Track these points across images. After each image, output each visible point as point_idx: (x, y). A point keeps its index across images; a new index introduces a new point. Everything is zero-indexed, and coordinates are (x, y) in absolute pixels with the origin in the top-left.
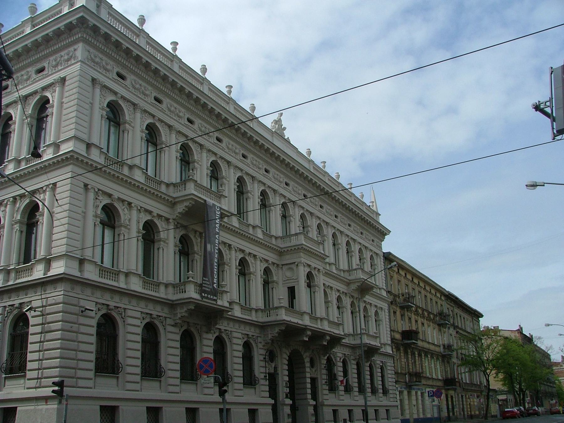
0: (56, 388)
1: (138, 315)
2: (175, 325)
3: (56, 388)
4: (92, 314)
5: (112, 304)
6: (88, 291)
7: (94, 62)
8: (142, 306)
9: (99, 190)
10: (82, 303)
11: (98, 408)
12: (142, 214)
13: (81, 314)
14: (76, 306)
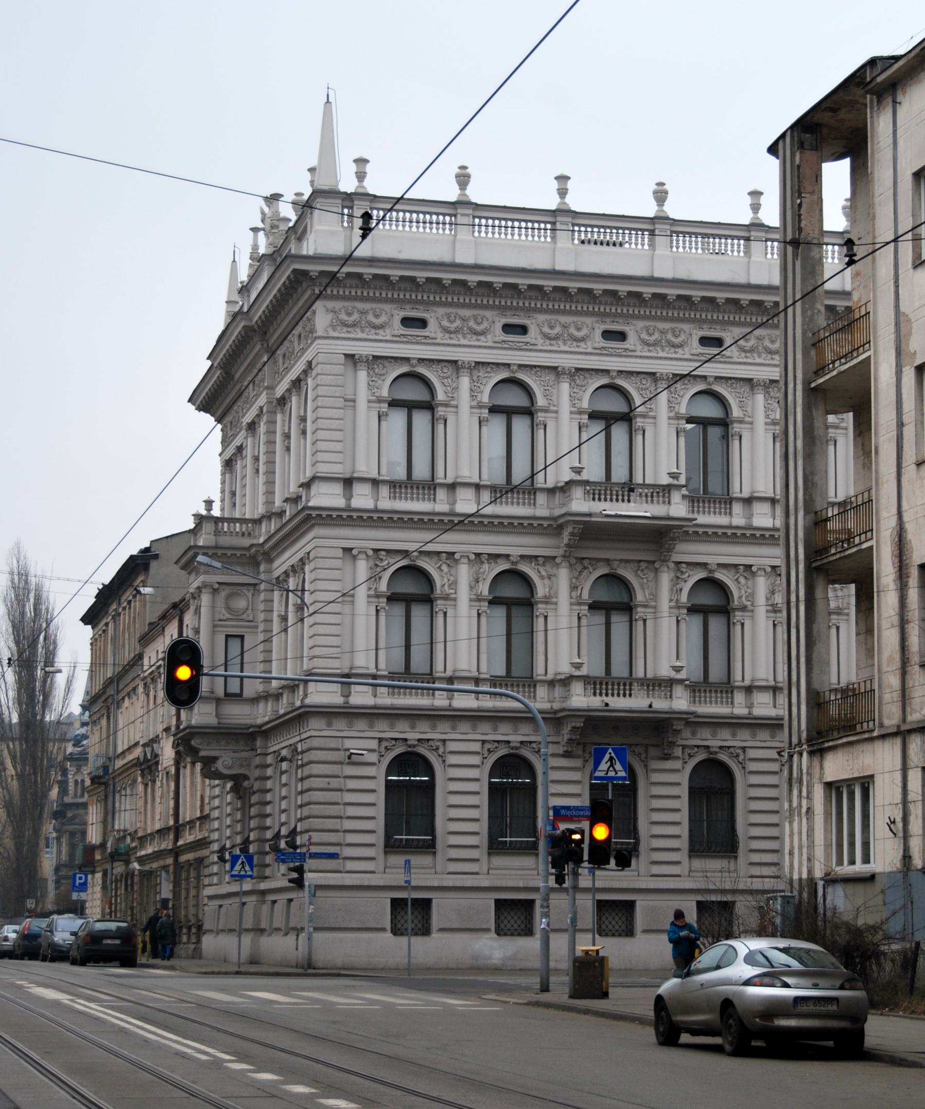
0: (295, 875)
1: (476, 747)
2: (567, 755)
3: (295, 875)
4: (373, 757)
5: (714, 743)
6: (361, 724)
7: (344, 324)
8: (486, 731)
9: (376, 551)
10: (348, 744)
11: (694, 904)
12: (486, 566)
13: (347, 761)
14: (338, 749)
